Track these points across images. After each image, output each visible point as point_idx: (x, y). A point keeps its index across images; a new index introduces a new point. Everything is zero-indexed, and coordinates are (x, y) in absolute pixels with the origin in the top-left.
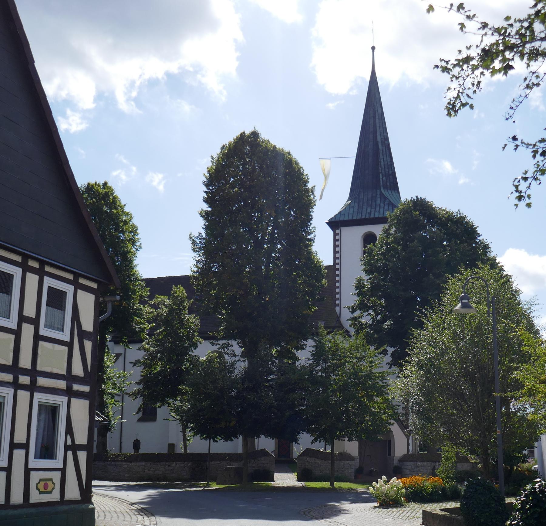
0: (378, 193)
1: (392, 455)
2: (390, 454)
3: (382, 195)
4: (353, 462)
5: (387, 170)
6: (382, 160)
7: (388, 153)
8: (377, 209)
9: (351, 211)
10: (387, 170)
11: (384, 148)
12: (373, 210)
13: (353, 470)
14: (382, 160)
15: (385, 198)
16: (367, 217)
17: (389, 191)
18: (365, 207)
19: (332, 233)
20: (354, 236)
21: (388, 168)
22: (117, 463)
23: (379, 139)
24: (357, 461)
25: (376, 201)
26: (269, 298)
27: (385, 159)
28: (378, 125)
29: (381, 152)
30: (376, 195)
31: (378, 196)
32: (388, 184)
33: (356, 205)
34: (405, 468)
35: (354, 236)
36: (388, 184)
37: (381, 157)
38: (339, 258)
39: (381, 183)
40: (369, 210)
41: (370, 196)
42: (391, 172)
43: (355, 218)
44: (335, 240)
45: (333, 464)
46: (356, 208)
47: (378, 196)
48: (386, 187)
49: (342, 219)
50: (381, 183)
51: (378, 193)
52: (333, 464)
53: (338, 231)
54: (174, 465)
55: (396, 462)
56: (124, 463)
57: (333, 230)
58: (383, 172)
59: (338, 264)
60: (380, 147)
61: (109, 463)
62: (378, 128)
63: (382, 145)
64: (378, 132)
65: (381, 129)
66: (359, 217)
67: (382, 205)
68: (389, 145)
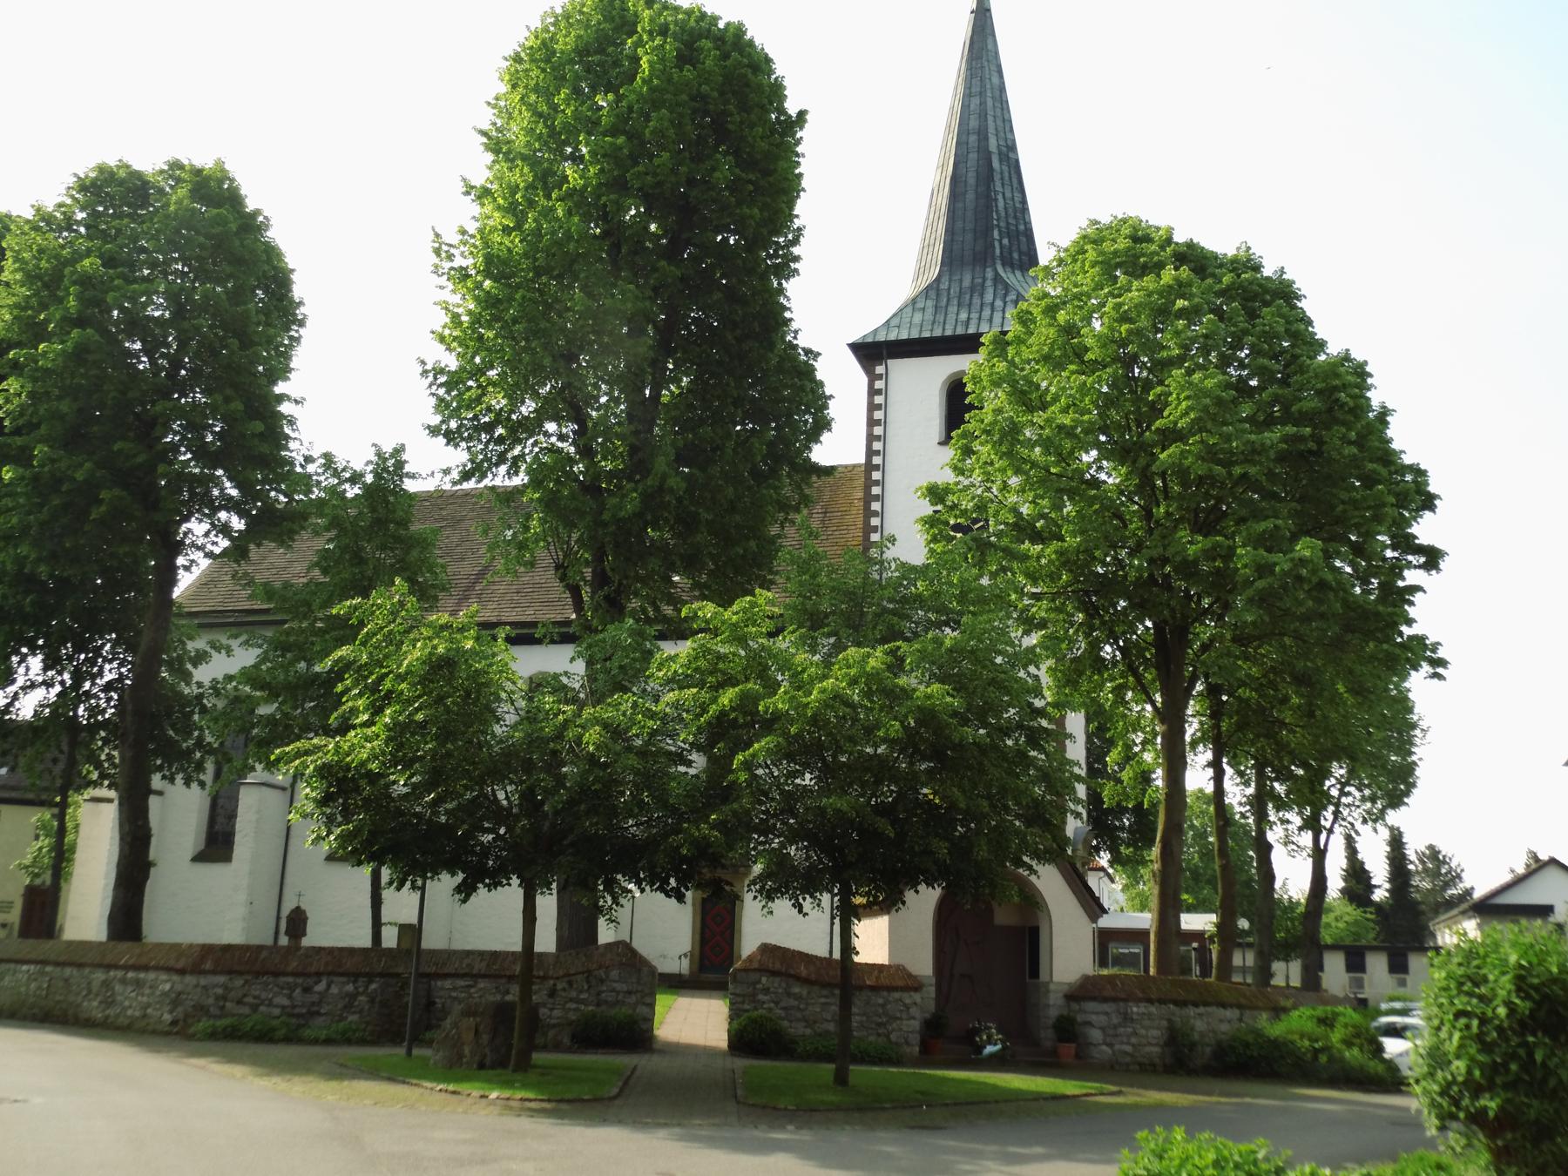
0: (990, 274)
1: (1044, 976)
2: (1035, 972)
3: (997, 279)
4: (917, 997)
5: (1012, 221)
6: (1000, 197)
7: (1015, 181)
8: (987, 313)
9: (918, 318)
10: (1012, 221)
11: (1005, 168)
12: (974, 316)
13: (916, 1025)
14: (1000, 197)
15: (1007, 288)
16: (960, 331)
17: (1018, 273)
18: (953, 309)
19: (864, 379)
20: (920, 385)
21: (1015, 217)
22: (142, 975)
23: (993, 144)
24: (931, 991)
25: (982, 296)
26: (259, 509)
27: (1008, 195)
28: (990, 112)
29: (997, 177)
30: (984, 279)
31: (989, 283)
32: (1016, 255)
33: (930, 303)
34: (1089, 1024)
35: (920, 385)
36: (1016, 255)
37: (999, 188)
38: (883, 423)
39: (998, 251)
40: (963, 316)
41: (967, 283)
42: (1022, 227)
43: (926, 334)
44: (873, 392)
45: (846, 1004)
46: (930, 311)
47: (989, 283)
48: (1008, 263)
49: (892, 337)
50: (998, 251)
51: (990, 274)
52: (846, 1004)
53: (880, 370)
54: (321, 987)
55: (1054, 1005)
56: (164, 977)
57: (864, 367)
58: (1002, 224)
59: (877, 453)
60: (996, 164)
61: (120, 974)
62: (990, 119)
63: (1001, 161)
64: (991, 130)
65: (999, 123)
66: (938, 333)
67: (999, 303)
68: (1017, 161)
